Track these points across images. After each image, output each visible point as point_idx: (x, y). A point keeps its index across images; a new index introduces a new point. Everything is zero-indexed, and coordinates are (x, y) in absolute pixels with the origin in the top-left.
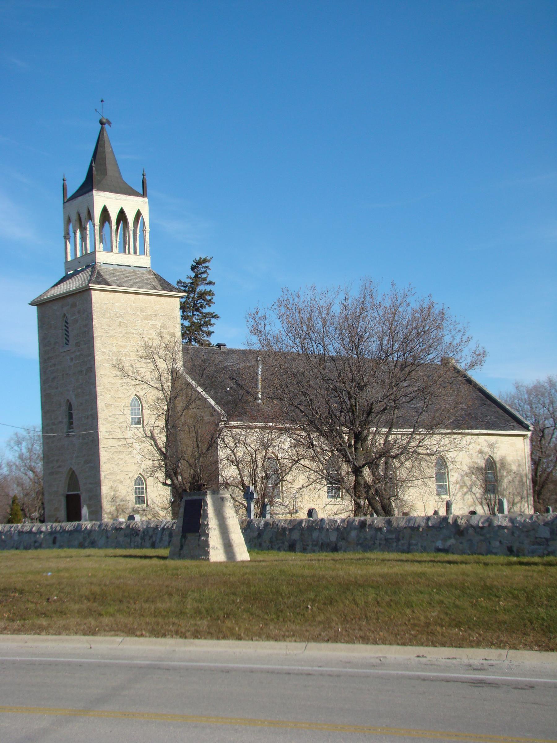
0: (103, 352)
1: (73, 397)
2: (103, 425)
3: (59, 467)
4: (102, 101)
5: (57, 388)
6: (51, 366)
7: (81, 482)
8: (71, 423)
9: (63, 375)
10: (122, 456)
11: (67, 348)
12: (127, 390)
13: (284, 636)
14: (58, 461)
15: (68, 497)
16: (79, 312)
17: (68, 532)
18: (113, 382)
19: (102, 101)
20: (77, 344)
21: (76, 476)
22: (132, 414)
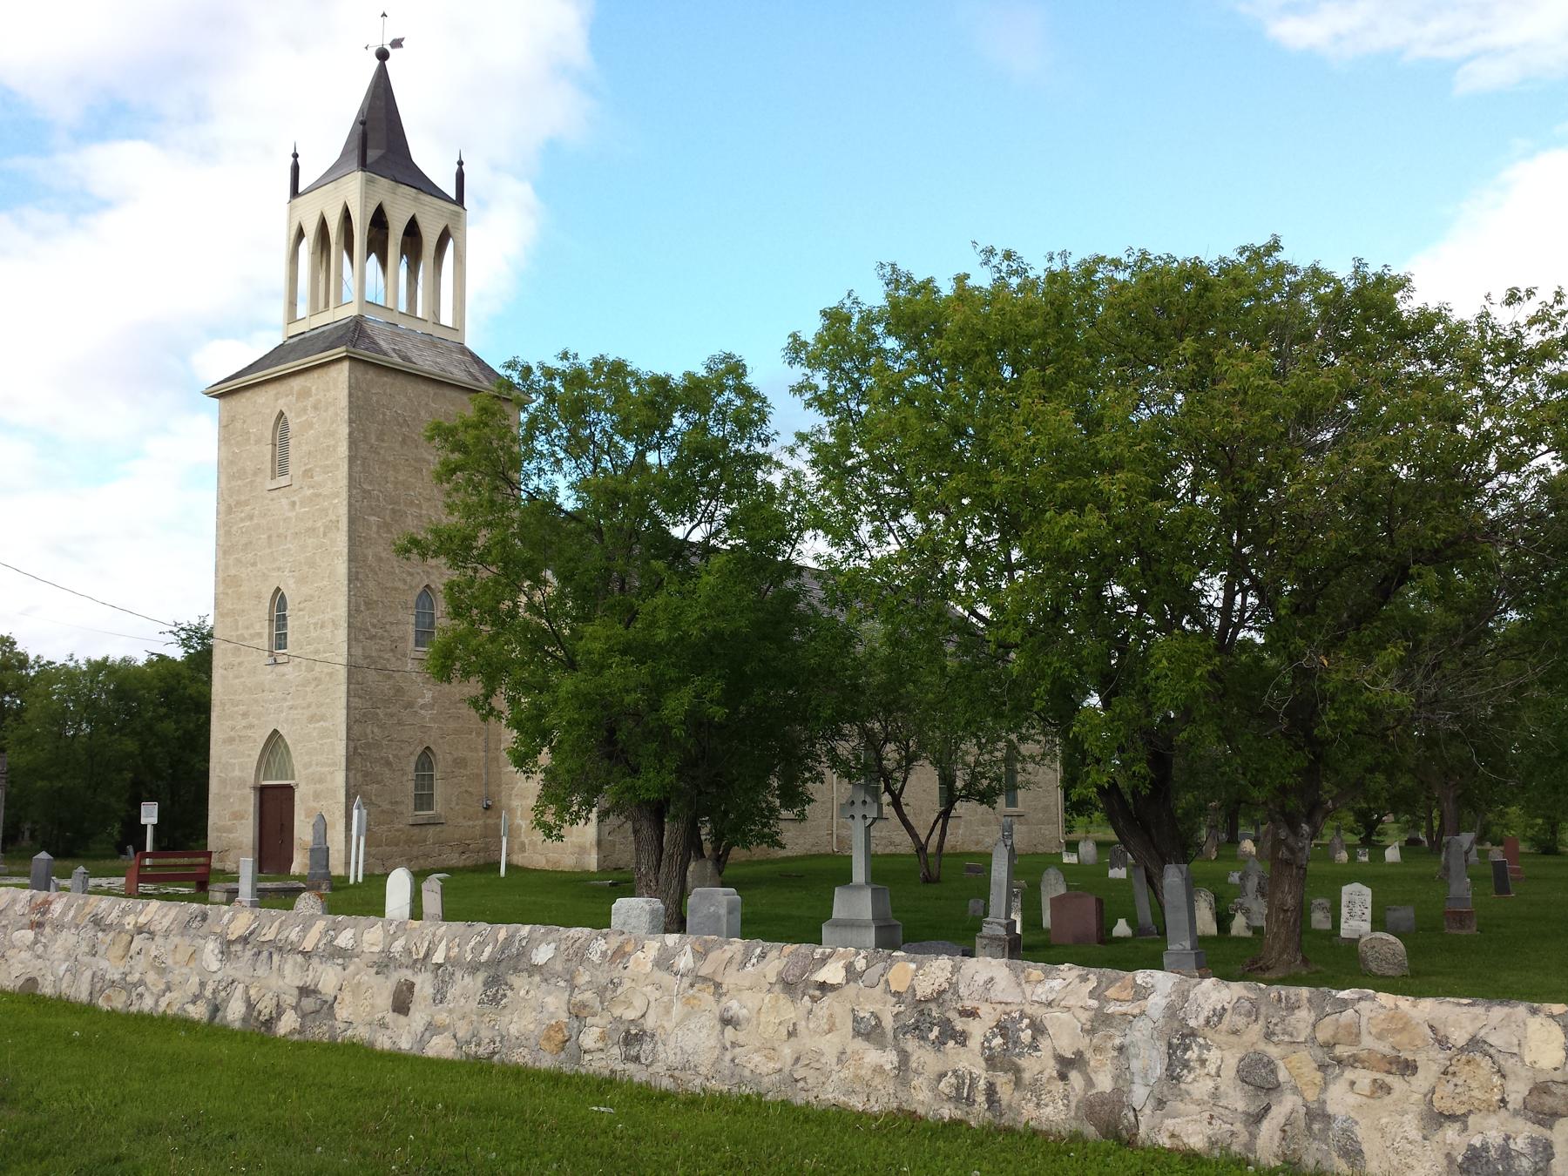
0: (365, 491)
1: (291, 582)
2: (237, 816)
3: (251, 726)
4: (384, 15)
5: (254, 564)
6: (242, 520)
7: (299, 759)
8: (280, 641)
9: (270, 537)
10: (393, 710)
11: (283, 481)
12: (411, 574)
13: (807, 1119)
14: (245, 715)
15: (263, 792)
16: (315, 408)
17: (566, 512)
18: (384, 555)
19: (384, 15)
20: (308, 473)
21: (286, 746)
22: (417, 624)
